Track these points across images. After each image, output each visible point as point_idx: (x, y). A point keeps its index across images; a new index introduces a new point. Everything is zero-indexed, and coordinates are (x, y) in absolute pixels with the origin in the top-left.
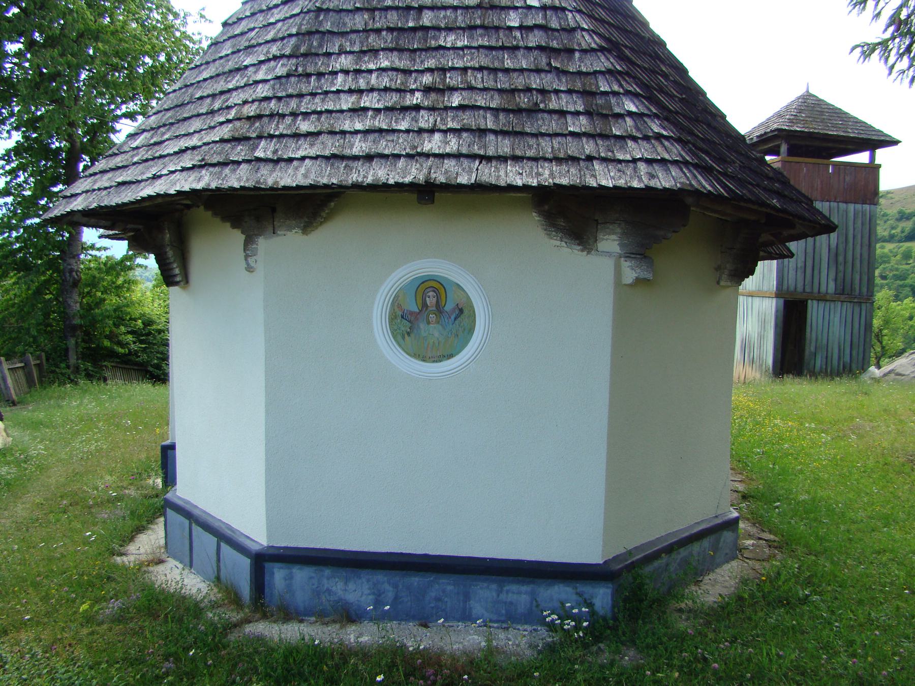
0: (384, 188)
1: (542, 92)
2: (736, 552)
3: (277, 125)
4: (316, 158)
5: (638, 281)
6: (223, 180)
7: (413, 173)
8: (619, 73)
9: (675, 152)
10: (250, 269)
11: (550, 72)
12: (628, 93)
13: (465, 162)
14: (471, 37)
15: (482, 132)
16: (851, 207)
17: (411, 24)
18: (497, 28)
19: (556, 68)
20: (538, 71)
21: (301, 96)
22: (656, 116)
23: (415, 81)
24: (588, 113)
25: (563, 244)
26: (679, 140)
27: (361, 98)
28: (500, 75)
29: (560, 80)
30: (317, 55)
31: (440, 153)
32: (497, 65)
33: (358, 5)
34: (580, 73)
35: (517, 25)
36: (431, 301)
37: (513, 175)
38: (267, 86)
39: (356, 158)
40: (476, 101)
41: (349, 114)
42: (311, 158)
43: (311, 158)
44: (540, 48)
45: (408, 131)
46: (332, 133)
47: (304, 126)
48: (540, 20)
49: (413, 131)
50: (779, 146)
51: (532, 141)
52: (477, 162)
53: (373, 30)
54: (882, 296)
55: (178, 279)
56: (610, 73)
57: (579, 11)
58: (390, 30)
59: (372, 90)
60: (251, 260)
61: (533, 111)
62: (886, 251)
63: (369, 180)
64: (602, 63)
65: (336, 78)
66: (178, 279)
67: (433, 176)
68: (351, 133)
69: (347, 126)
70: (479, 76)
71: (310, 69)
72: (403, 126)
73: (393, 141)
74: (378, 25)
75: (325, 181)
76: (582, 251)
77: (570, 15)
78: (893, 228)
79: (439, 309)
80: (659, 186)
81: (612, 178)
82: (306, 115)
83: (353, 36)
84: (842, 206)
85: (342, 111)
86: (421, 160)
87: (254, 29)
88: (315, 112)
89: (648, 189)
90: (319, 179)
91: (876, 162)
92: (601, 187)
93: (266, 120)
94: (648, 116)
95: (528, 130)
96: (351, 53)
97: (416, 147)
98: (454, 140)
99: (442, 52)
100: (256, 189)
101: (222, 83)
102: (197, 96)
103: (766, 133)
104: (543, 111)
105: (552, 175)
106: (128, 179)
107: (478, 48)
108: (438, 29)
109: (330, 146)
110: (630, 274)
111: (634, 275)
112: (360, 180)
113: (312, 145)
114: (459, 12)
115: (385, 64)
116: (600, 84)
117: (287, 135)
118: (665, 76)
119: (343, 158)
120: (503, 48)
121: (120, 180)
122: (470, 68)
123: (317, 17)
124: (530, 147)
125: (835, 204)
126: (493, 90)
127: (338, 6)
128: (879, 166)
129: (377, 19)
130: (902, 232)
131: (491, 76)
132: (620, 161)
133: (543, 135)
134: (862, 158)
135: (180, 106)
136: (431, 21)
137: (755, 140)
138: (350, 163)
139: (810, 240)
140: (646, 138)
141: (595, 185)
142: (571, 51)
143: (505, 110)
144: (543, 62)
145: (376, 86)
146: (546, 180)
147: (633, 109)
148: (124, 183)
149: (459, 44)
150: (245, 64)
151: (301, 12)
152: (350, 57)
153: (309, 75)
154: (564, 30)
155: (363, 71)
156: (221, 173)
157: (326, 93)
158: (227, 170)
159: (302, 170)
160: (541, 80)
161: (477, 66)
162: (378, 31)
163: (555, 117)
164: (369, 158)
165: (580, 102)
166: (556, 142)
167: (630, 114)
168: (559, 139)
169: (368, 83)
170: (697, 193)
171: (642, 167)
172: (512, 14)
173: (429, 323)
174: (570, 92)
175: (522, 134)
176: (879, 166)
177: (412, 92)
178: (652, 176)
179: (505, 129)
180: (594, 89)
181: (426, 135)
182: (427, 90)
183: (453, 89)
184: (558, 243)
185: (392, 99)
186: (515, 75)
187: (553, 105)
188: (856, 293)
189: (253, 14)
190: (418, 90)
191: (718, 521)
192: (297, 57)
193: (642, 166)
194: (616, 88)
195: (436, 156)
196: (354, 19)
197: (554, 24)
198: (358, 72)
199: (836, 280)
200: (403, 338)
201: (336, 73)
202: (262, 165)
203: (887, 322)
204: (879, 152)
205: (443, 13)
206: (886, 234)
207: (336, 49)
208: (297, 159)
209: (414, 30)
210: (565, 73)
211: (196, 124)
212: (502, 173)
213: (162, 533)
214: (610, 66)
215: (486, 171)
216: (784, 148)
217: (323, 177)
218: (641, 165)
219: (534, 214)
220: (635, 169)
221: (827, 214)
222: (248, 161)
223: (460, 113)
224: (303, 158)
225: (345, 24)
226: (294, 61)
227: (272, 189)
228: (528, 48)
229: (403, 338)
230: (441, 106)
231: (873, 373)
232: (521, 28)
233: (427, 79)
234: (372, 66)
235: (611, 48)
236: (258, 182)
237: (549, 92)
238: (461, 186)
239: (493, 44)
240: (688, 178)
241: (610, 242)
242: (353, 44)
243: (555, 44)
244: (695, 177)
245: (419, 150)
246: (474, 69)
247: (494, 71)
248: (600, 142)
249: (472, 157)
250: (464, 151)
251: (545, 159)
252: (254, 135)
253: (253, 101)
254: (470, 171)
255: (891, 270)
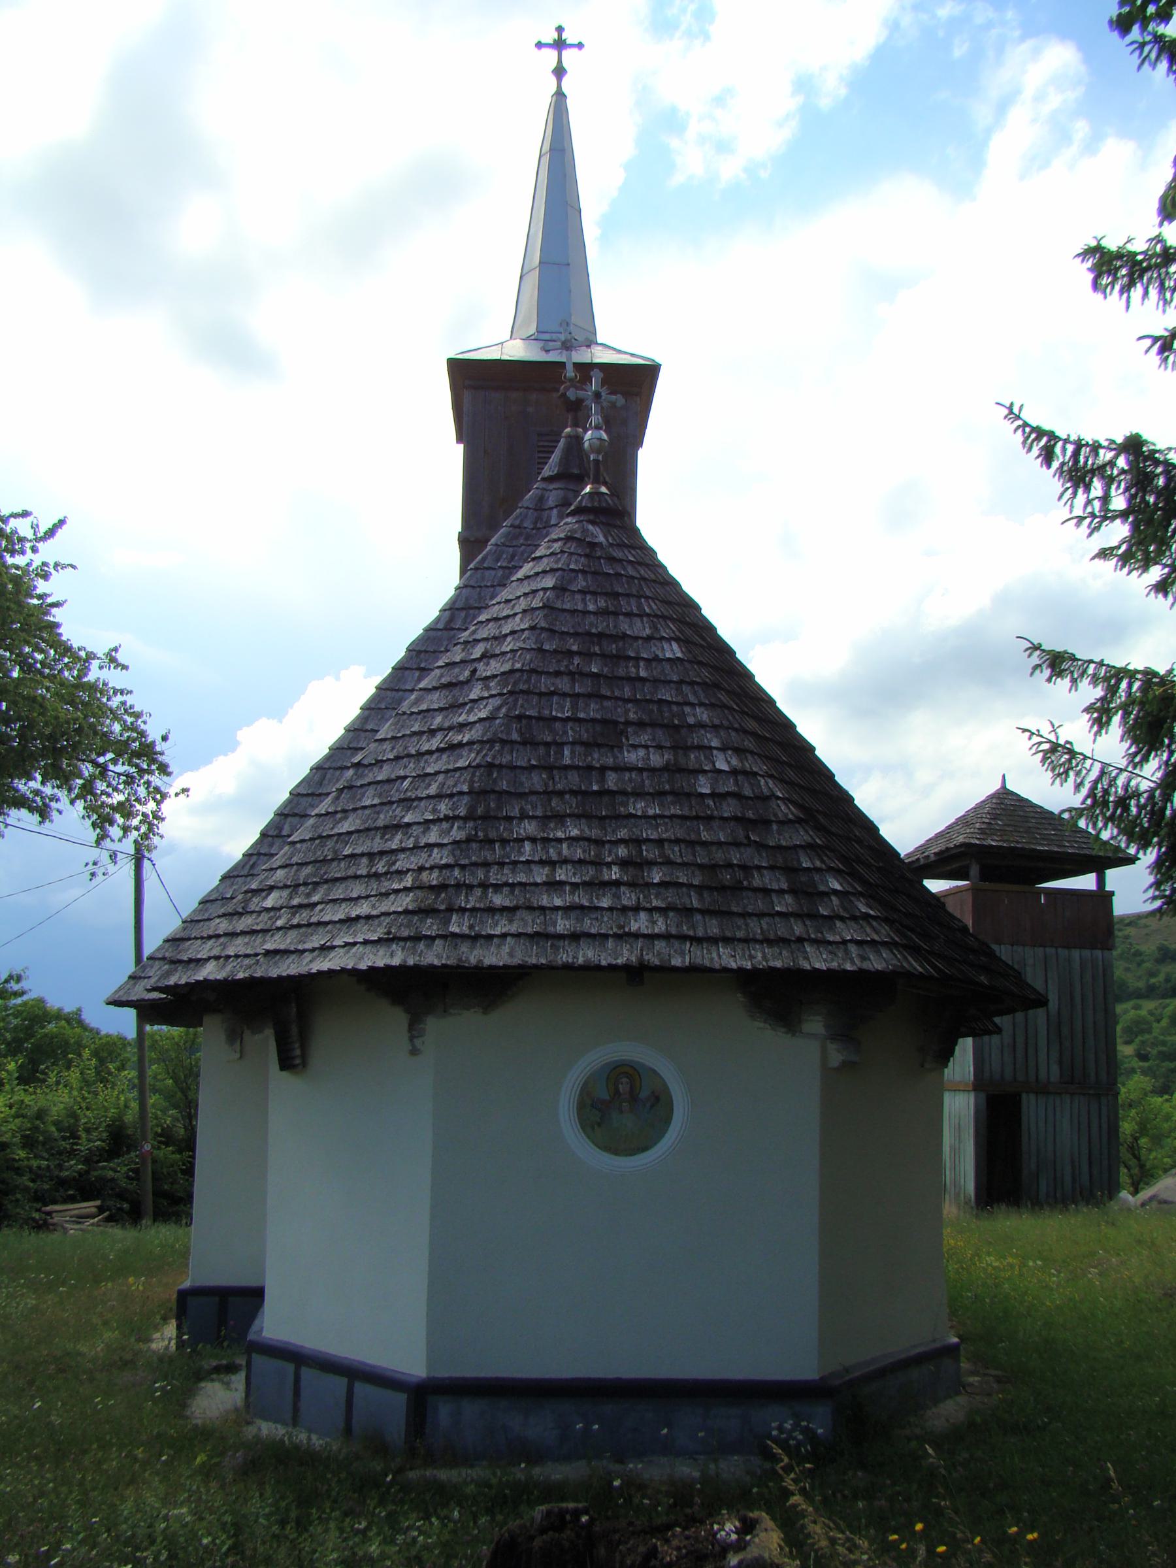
0: (591, 969)
1: (744, 867)
2: (958, 1387)
3: (466, 897)
4: (518, 936)
5: (846, 1065)
6: (420, 956)
7: (626, 955)
8: (819, 846)
9: (884, 933)
10: (414, 1052)
11: (749, 845)
12: (830, 869)
13: (676, 944)
14: (661, 805)
15: (688, 911)
16: (1076, 954)
17: (595, 788)
18: (688, 795)
19: (755, 842)
20: (737, 844)
21: (486, 865)
22: (861, 894)
23: (610, 852)
24: (792, 891)
25: (767, 1026)
26: (886, 920)
27: (554, 870)
28: (698, 848)
29: (760, 855)
30: (496, 818)
31: (645, 931)
32: (693, 837)
33: (533, 762)
34: (779, 847)
35: (708, 791)
36: (623, 1088)
37: (726, 958)
38: (445, 852)
39: (561, 937)
40: (678, 877)
41: (545, 888)
42: (513, 935)
43: (513, 935)
44: (736, 819)
45: (611, 909)
46: (530, 908)
47: (498, 900)
48: (730, 786)
49: (617, 909)
50: (967, 867)
51: (740, 922)
52: (688, 945)
53: (553, 792)
54: (1133, 1086)
55: (298, 1061)
56: (810, 847)
57: (771, 776)
58: (573, 793)
59: (565, 861)
60: (417, 1042)
61: (737, 888)
62: (1143, 1013)
63: (581, 960)
64: (801, 836)
65: (523, 846)
66: (298, 1061)
67: (646, 958)
68: (550, 909)
69: (545, 901)
70: (676, 849)
71: (493, 835)
72: (605, 903)
73: (597, 919)
74: (559, 787)
75: (534, 961)
76: (787, 1033)
77: (762, 782)
78: (1152, 974)
79: (633, 1098)
80: (871, 968)
81: (825, 960)
82: (497, 887)
83: (533, 798)
84: (1063, 952)
85: (536, 884)
86: (631, 940)
87: (405, 777)
88: (506, 884)
89: (861, 971)
90: (527, 959)
91: (1107, 889)
92: (816, 970)
93: (451, 890)
94: (852, 894)
95: (735, 909)
96: (533, 817)
97: (623, 927)
98: (661, 920)
99: (633, 820)
100: (458, 967)
101: (378, 840)
102: (346, 853)
103: (948, 849)
104: (747, 889)
105: (764, 957)
106: (282, 947)
107: (671, 817)
108: (624, 793)
109: (532, 924)
110: (836, 1057)
111: (841, 1058)
112: (570, 961)
113: (511, 921)
114: (645, 774)
115: (575, 832)
116: (802, 859)
117: (479, 909)
118: (859, 841)
119: (547, 936)
120: (697, 818)
121: (269, 946)
122: (666, 840)
123: (490, 774)
124: (739, 928)
125: (1053, 950)
126: (693, 865)
127: (511, 761)
128: (1112, 893)
129: (557, 779)
130: (1167, 980)
131: (689, 850)
132: (830, 943)
133: (750, 915)
134: (1086, 882)
135: (321, 861)
136: (616, 784)
137: (932, 858)
138: (556, 942)
139: (1020, 1016)
140: (854, 918)
141: (809, 968)
142: (767, 823)
143: (711, 889)
144: (741, 834)
145: (569, 857)
146: (760, 963)
147: (838, 887)
148: (276, 952)
149: (651, 812)
150: (406, 820)
151: (469, 766)
152: (534, 823)
153: (492, 842)
154: (757, 798)
155: (552, 840)
156: (414, 947)
157: (515, 863)
158: (422, 946)
159: (506, 949)
160: (741, 854)
161: (673, 837)
162: (561, 794)
163: (760, 895)
164: (575, 937)
165: (783, 879)
166: (764, 922)
167: (835, 892)
168: (767, 919)
169: (560, 853)
170: (908, 975)
171: (853, 949)
172: (702, 779)
173: (621, 1112)
174: (772, 868)
175: (730, 914)
176: (1112, 893)
177: (609, 865)
178: (863, 958)
179: (712, 908)
180: (795, 864)
181: (630, 913)
182: (624, 864)
183: (651, 863)
184: (762, 1025)
185: (589, 873)
186: (714, 848)
187: (757, 882)
188: (1094, 1081)
189: (398, 758)
190: (615, 864)
191: (938, 1345)
192: (475, 820)
193: (853, 948)
194: (818, 864)
195: (645, 936)
196: (532, 779)
197: (747, 792)
198: (546, 840)
199: (1061, 1063)
200: (593, 1129)
201: (522, 840)
202: (459, 941)
203: (1143, 1128)
204: (1110, 874)
205: (627, 775)
206: (1141, 984)
207: (516, 812)
208: (497, 936)
209: (599, 793)
210: (766, 847)
211: (357, 890)
212: (715, 955)
213: (242, 1387)
214: (809, 840)
215: (699, 953)
216: (974, 870)
217: (530, 956)
218: (851, 947)
219: (739, 995)
220: (847, 952)
221: (1042, 992)
222: (443, 937)
223: (662, 890)
224: (504, 936)
225: (522, 784)
226: (471, 824)
227: (476, 967)
228: (722, 818)
229: (593, 1129)
230: (641, 881)
231: (1125, 1201)
232: (713, 795)
233: (622, 851)
234: (560, 834)
235: (808, 818)
236: (460, 960)
237: (750, 868)
238: (675, 969)
239: (686, 812)
240: (899, 960)
241: (815, 1025)
242: (534, 808)
243: (750, 814)
244: (906, 958)
245: (627, 930)
246: (670, 841)
247: (691, 844)
248: (808, 923)
249: (683, 938)
250: (673, 931)
251: (756, 941)
252: (443, 907)
253: (432, 868)
254: (683, 954)
255: (1154, 1045)
